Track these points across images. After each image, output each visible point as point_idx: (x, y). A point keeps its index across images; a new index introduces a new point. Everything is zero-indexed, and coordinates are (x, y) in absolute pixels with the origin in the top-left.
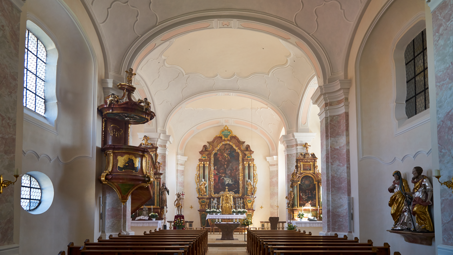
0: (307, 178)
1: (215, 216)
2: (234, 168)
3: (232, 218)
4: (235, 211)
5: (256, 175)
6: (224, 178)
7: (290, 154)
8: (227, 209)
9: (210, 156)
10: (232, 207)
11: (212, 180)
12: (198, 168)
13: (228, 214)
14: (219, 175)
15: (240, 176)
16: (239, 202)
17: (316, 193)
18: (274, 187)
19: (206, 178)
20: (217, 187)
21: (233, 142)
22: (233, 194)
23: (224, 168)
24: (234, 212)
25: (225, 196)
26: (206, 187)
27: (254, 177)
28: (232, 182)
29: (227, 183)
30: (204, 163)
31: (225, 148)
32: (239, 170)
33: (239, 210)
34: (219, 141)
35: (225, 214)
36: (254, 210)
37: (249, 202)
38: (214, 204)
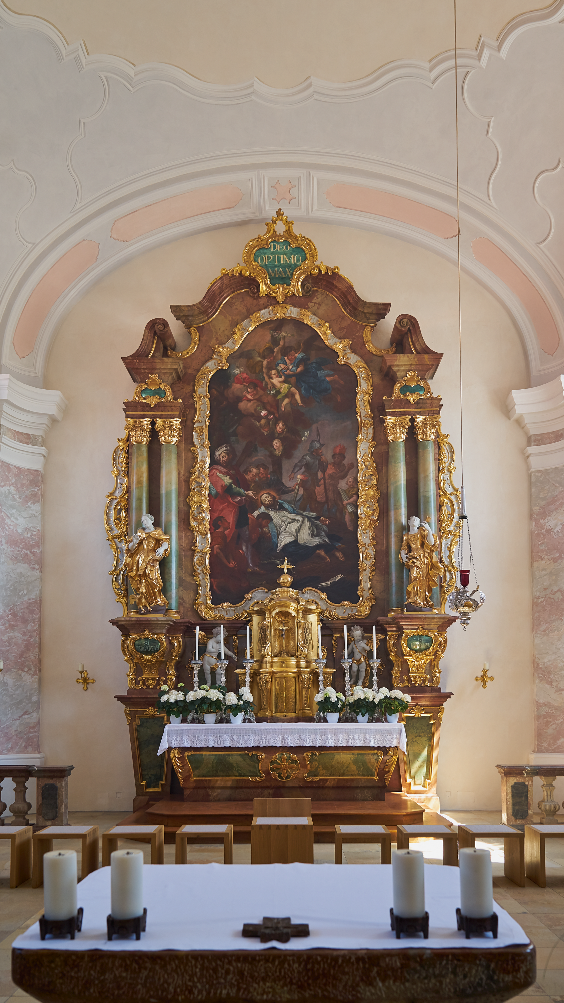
1: (217, 734)
2: (328, 455)
3: (318, 745)
4: (334, 699)
5: (453, 498)
6: (272, 513)
8: (288, 689)
9: (188, 389)
10: (315, 674)
11: (201, 522)
12: (123, 456)
13: (291, 720)
14: (240, 495)
15: (361, 499)
16: (356, 651)
18: (555, 560)
19: (169, 513)
20: (232, 564)
21: (321, 311)
22: (320, 603)
23: (272, 454)
25: (274, 613)
26: (164, 563)
27: (440, 507)
28: (313, 535)
30: (153, 423)
31: (275, 341)
32: (354, 465)
33: (360, 693)
34: (239, 306)
35: (273, 720)
36: (448, 696)
37: (417, 645)
38: (213, 661)
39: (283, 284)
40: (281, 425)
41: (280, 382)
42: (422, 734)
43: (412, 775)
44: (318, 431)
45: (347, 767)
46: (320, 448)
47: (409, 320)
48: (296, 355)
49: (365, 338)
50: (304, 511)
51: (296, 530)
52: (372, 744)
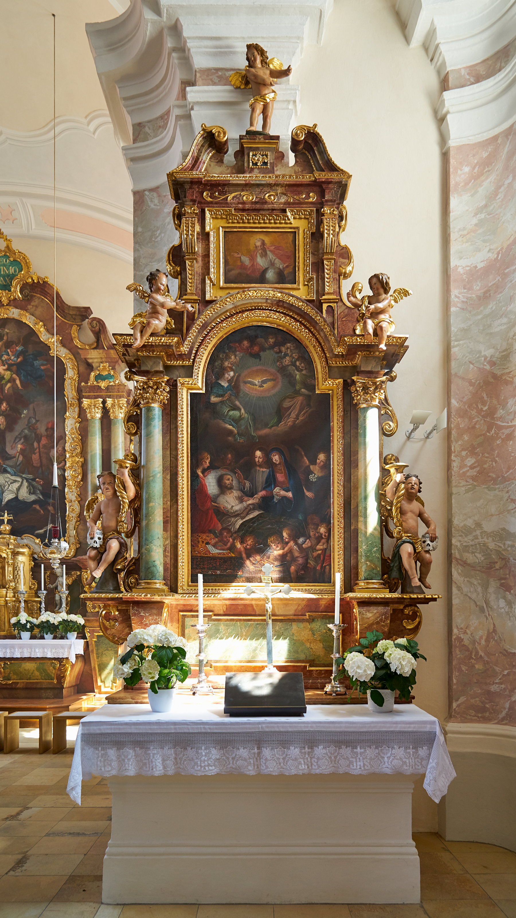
0: (263, 349)
2: (42, 429)
3: (8, 656)
7: (151, 190)
15: (68, 465)
17: (327, 466)
24: (21, 627)
28: (30, 493)
29: (11, 496)
33: (46, 616)
39: (5, 290)
40: (4, 404)
41: (4, 370)
42: (110, 649)
43: (103, 680)
44: (34, 409)
45: (32, 673)
46: (35, 424)
47: (97, 321)
48: (17, 348)
49: (72, 335)
50: (23, 474)
51: (17, 489)
52: (49, 656)
